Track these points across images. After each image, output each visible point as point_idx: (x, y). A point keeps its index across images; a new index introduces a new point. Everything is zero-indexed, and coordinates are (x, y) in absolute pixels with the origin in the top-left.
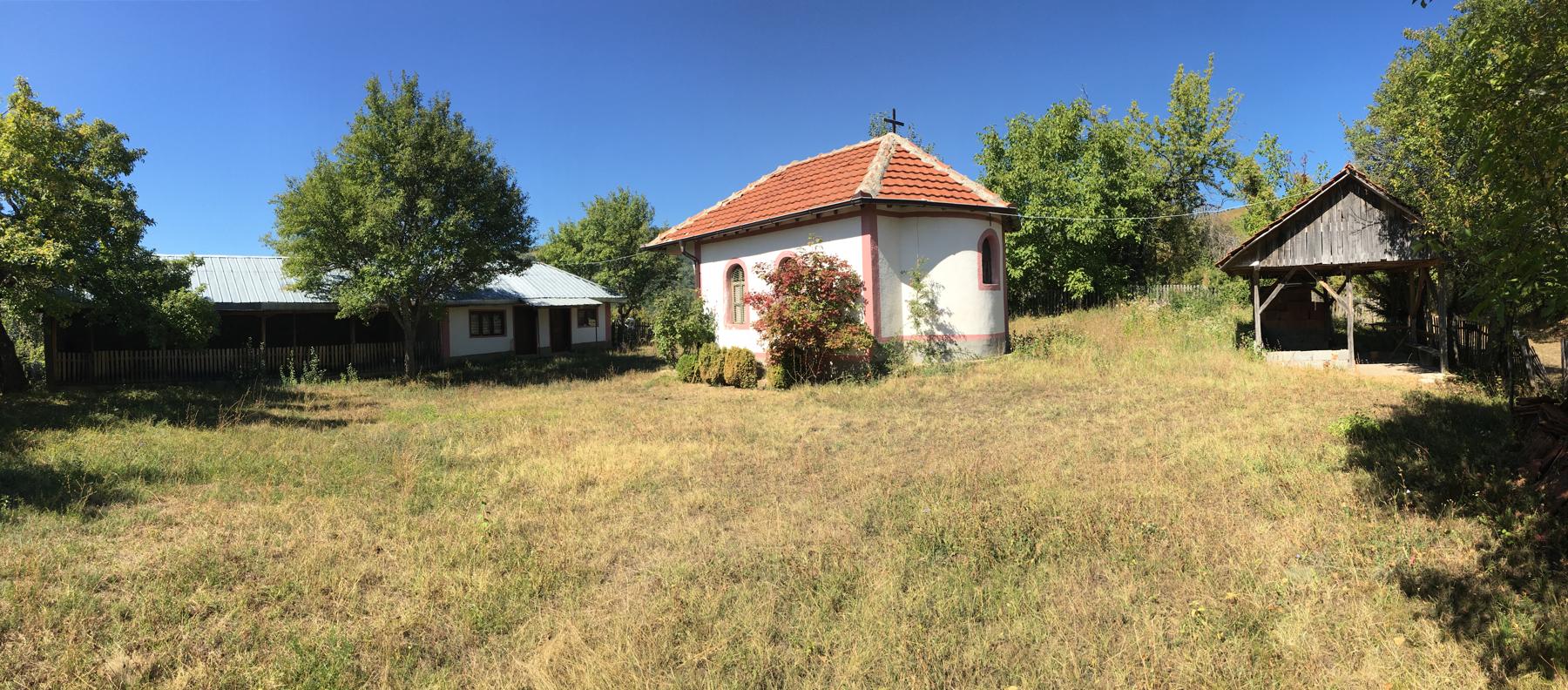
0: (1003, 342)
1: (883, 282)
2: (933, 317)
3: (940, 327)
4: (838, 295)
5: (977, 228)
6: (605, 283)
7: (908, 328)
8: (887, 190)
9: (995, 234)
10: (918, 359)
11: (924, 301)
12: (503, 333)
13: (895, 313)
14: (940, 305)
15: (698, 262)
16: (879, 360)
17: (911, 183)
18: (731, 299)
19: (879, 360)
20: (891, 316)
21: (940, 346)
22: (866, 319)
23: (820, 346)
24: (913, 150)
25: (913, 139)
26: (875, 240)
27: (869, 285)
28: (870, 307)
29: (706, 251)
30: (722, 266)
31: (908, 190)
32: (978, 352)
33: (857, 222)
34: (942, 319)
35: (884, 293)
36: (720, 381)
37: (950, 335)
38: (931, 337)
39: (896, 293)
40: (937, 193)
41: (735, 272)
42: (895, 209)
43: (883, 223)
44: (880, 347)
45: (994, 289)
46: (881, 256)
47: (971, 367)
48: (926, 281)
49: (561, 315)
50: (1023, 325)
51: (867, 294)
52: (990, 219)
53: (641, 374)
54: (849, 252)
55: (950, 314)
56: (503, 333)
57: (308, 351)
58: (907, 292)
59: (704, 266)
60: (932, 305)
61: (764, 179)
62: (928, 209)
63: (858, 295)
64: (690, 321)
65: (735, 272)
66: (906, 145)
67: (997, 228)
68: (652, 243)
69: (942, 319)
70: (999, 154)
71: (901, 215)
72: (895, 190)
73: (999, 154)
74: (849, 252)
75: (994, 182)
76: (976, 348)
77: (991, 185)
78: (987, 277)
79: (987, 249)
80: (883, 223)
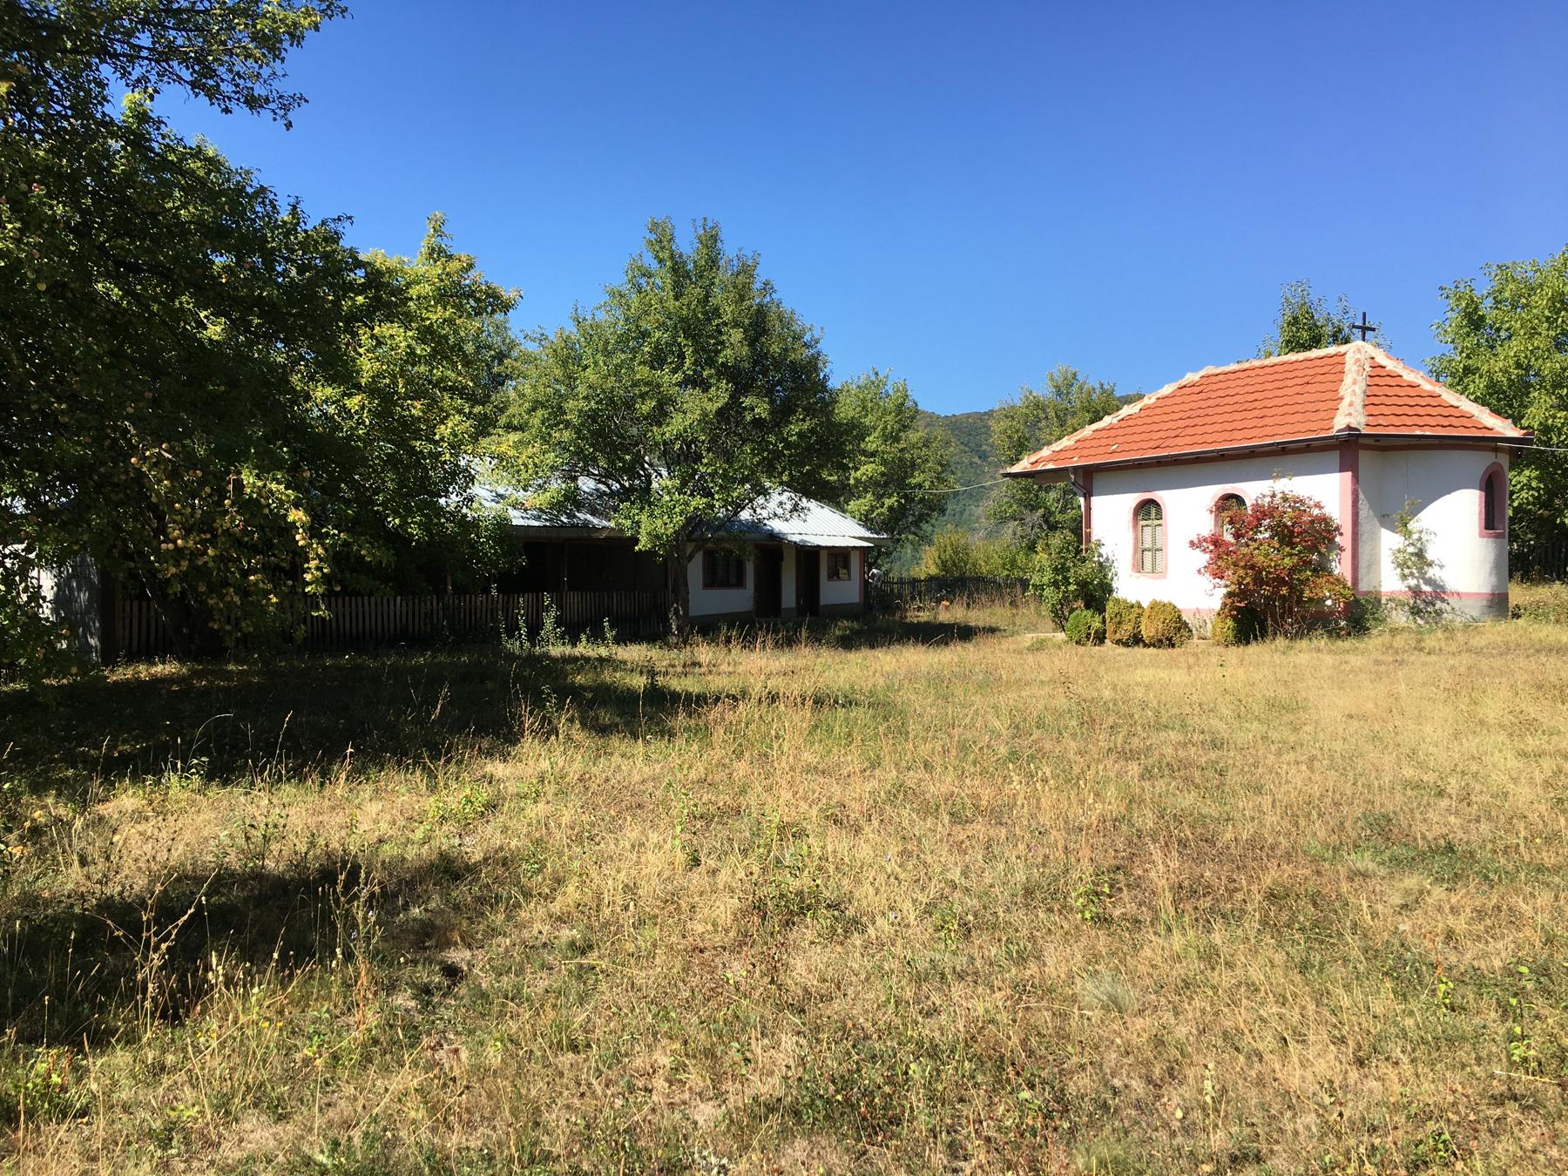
0: (1499, 604)
1: (1365, 527)
2: (1420, 570)
3: (1429, 582)
4: (1308, 537)
5: (1479, 463)
6: (866, 521)
7: (1389, 581)
8: (1372, 420)
9: (1491, 466)
10: (1400, 618)
11: (1411, 549)
12: (740, 583)
13: (1374, 563)
14: (1429, 556)
15: (1088, 495)
16: (1358, 616)
17: (1399, 411)
18: (1138, 541)
19: (1358, 616)
20: (1369, 566)
21: (1427, 603)
22: (1341, 567)
23: (1281, 594)
24: (1391, 365)
25: (1389, 350)
26: (1356, 478)
27: (1347, 529)
28: (1347, 556)
29: (1098, 480)
30: (1132, 499)
31: (1396, 421)
32: (1476, 614)
33: (1335, 456)
34: (1432, 572)
35: (1363, 538)
36: (1136, 640)
37: (1440, 592)
38: (1416, 592)
39: (1375, 539)
40: (1432, 422)
41: (1148, 510)
42: (1382, 443)
43: (1365, 458)
44: (1357, 601)
45: (1498, 536)
46: (1361, 496)
47: (1470, 626)
48: (1412, 525)
49: (809, 555)
50: (1518, 594)
51: (1344, 540)
52: (1496, 450)
53: (921, 648)
54: (1326, 491)
55: (1442, 567)
56: (740, 583)
57: (540, 601)
58: (1389, 541)
59: (1095, 500)
60: (1420, 554)
61: (1168, 389)
62: (1423, 441)
63: (1332, 541)
64: (1085, 571)
65: (1148, 510)
66: (1381, 358)
67: (1504, 460)
68: (1017, 469)
69: (1432, 572)
70: (1474, 321)
71: (1385, 449)
72: (1381, 421)
73: (1474, 321)
74: (1326, 491)
75: (1468, 370)
76: (1473, 609)
77: (1461, 378)
78: (1490, 520)
79: (1492, 488)
80: (1365, 458)
